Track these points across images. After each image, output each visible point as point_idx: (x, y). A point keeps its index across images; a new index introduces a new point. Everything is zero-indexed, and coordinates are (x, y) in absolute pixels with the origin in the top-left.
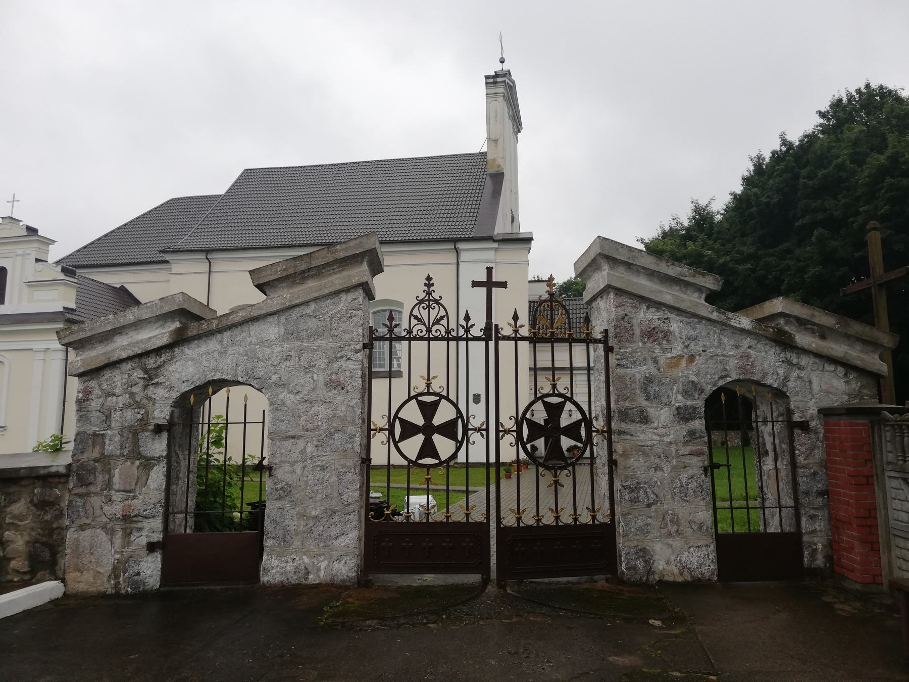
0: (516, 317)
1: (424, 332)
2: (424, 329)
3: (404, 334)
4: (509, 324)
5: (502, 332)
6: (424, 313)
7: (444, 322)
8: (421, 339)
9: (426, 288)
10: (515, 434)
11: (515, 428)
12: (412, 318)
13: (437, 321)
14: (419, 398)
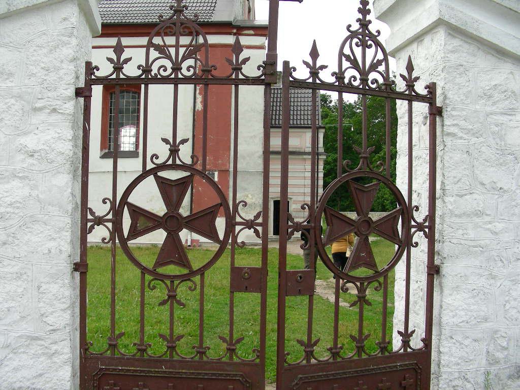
0: (314, 53)
1: (169, 71)
2: (169, 64)
3: (332, 80)
4: (305, 63)
5: (294, 74)
6: (358, 51)
7: (382, 68)
8: (165, 80)
9: (360, 16)
10: (110, 225)
11: (110, 216)
12: (344, 59)
13: (374, 67)
14: (160, 174)
